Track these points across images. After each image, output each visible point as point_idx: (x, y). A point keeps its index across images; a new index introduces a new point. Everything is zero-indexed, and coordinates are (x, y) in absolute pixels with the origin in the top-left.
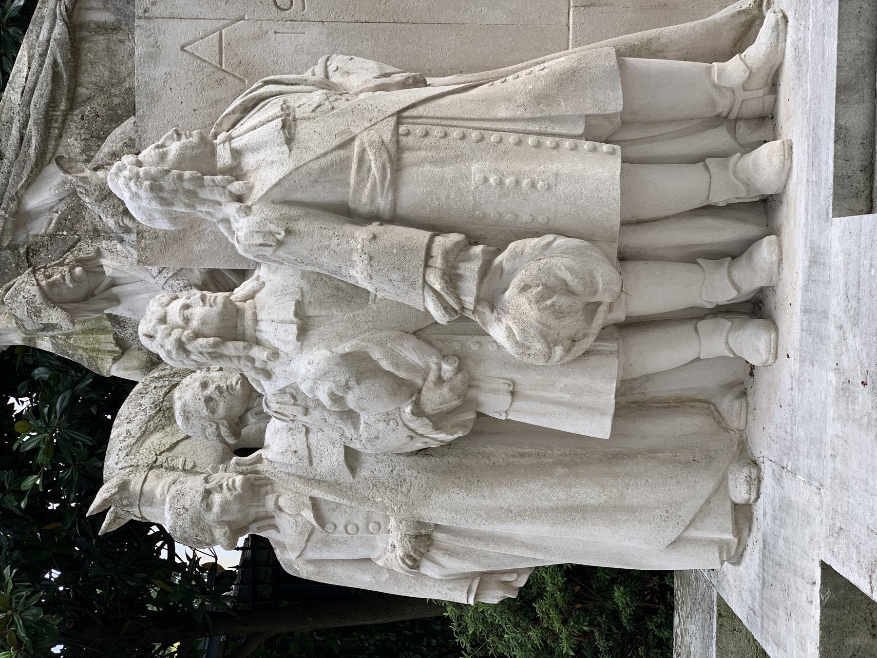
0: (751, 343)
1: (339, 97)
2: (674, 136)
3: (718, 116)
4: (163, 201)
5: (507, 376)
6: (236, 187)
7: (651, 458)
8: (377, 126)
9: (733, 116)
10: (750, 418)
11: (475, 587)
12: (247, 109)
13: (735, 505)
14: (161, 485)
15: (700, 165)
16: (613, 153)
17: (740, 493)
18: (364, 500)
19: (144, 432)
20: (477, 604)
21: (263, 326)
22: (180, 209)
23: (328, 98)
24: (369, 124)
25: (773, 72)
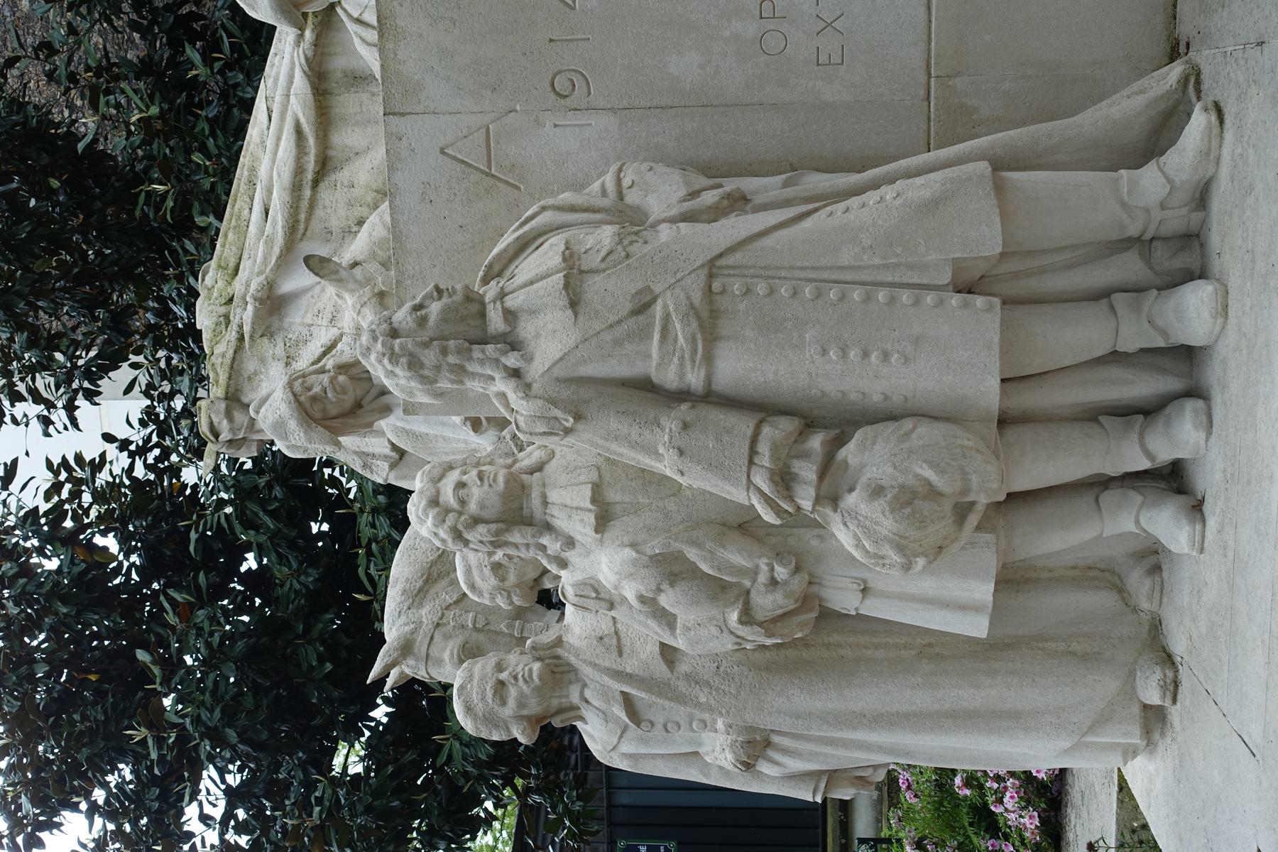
0: (1165, 523)
1: (635, 238)
2: (1069, 267)
3: (1129, 239)
4: (424, 379)
5: (855, 574)
6: (512, 360)
7: (1039, 649)
8: (683, 283)
9: (1148, 236)
10: (1165, 600)
11: (822, 785)
12: (522, 247)
13: (1146, 707)
14: (449, 648)
15: (1104, 301)
16: (990, 309)
17: (1153, 696)
18: (680, 699)
19: (427, 580)
20: (825, 800)
21: (554, 510)
22: (444, 385)
23: (621, 242)
24: (673, 281)
25: (1203, 183)
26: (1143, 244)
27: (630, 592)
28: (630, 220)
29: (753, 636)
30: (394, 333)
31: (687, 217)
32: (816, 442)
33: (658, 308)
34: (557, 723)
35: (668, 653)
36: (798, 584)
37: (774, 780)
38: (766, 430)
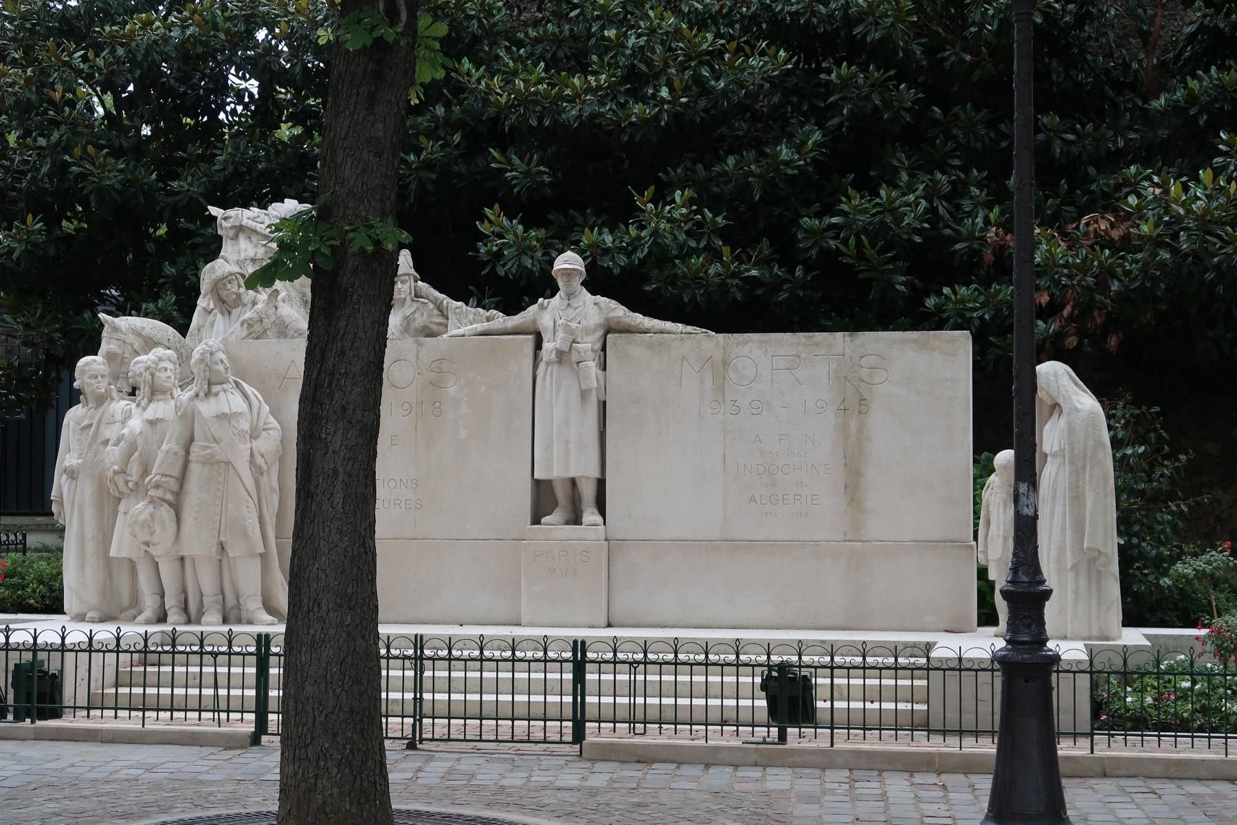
26: (238, 606)
27: (125, 431)
28: (254, 435)
29: (110, 474)
30: (212, 354)
32: (169, 497)
34: (82, 397)
35: (106, 442)
37: (61, 485)
38: (173, 480)
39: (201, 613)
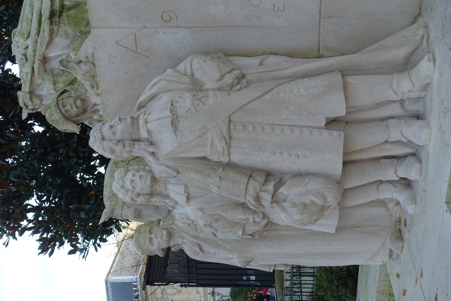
20: (274, 271)
31: (219, 89)
32: (270, 187)
33: (209, 135)
36: (264, 222)
39: (409, 143)
